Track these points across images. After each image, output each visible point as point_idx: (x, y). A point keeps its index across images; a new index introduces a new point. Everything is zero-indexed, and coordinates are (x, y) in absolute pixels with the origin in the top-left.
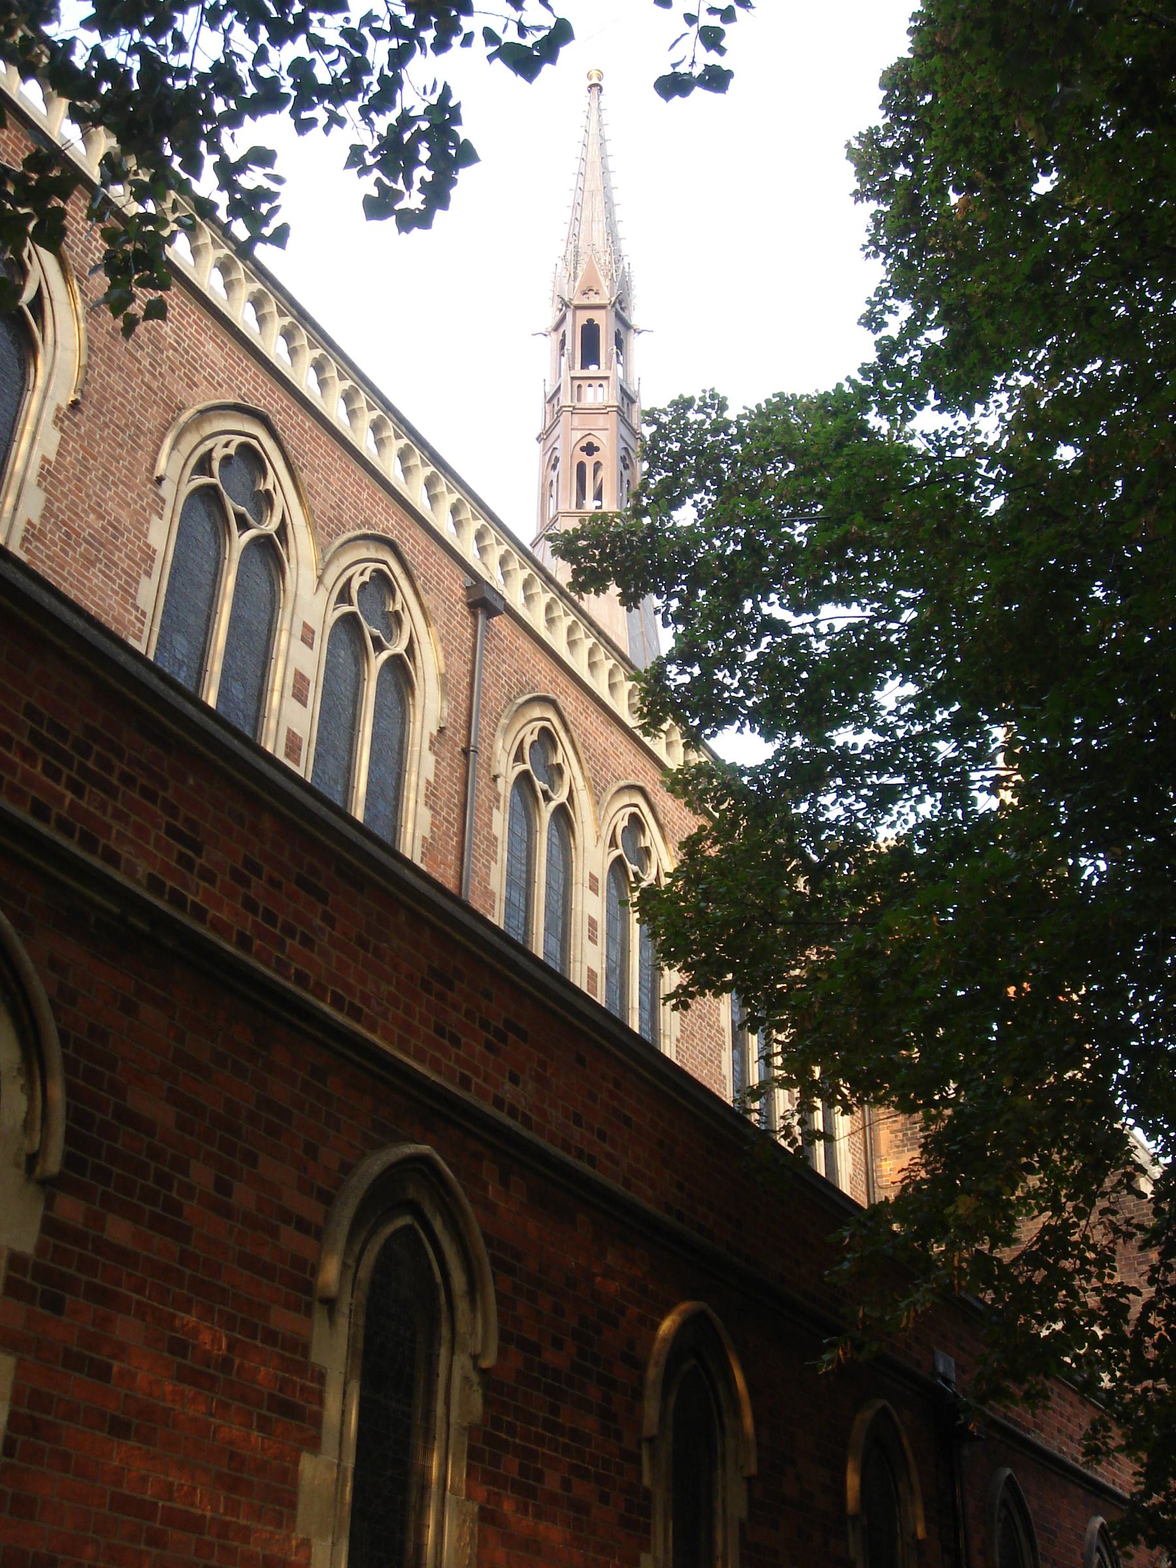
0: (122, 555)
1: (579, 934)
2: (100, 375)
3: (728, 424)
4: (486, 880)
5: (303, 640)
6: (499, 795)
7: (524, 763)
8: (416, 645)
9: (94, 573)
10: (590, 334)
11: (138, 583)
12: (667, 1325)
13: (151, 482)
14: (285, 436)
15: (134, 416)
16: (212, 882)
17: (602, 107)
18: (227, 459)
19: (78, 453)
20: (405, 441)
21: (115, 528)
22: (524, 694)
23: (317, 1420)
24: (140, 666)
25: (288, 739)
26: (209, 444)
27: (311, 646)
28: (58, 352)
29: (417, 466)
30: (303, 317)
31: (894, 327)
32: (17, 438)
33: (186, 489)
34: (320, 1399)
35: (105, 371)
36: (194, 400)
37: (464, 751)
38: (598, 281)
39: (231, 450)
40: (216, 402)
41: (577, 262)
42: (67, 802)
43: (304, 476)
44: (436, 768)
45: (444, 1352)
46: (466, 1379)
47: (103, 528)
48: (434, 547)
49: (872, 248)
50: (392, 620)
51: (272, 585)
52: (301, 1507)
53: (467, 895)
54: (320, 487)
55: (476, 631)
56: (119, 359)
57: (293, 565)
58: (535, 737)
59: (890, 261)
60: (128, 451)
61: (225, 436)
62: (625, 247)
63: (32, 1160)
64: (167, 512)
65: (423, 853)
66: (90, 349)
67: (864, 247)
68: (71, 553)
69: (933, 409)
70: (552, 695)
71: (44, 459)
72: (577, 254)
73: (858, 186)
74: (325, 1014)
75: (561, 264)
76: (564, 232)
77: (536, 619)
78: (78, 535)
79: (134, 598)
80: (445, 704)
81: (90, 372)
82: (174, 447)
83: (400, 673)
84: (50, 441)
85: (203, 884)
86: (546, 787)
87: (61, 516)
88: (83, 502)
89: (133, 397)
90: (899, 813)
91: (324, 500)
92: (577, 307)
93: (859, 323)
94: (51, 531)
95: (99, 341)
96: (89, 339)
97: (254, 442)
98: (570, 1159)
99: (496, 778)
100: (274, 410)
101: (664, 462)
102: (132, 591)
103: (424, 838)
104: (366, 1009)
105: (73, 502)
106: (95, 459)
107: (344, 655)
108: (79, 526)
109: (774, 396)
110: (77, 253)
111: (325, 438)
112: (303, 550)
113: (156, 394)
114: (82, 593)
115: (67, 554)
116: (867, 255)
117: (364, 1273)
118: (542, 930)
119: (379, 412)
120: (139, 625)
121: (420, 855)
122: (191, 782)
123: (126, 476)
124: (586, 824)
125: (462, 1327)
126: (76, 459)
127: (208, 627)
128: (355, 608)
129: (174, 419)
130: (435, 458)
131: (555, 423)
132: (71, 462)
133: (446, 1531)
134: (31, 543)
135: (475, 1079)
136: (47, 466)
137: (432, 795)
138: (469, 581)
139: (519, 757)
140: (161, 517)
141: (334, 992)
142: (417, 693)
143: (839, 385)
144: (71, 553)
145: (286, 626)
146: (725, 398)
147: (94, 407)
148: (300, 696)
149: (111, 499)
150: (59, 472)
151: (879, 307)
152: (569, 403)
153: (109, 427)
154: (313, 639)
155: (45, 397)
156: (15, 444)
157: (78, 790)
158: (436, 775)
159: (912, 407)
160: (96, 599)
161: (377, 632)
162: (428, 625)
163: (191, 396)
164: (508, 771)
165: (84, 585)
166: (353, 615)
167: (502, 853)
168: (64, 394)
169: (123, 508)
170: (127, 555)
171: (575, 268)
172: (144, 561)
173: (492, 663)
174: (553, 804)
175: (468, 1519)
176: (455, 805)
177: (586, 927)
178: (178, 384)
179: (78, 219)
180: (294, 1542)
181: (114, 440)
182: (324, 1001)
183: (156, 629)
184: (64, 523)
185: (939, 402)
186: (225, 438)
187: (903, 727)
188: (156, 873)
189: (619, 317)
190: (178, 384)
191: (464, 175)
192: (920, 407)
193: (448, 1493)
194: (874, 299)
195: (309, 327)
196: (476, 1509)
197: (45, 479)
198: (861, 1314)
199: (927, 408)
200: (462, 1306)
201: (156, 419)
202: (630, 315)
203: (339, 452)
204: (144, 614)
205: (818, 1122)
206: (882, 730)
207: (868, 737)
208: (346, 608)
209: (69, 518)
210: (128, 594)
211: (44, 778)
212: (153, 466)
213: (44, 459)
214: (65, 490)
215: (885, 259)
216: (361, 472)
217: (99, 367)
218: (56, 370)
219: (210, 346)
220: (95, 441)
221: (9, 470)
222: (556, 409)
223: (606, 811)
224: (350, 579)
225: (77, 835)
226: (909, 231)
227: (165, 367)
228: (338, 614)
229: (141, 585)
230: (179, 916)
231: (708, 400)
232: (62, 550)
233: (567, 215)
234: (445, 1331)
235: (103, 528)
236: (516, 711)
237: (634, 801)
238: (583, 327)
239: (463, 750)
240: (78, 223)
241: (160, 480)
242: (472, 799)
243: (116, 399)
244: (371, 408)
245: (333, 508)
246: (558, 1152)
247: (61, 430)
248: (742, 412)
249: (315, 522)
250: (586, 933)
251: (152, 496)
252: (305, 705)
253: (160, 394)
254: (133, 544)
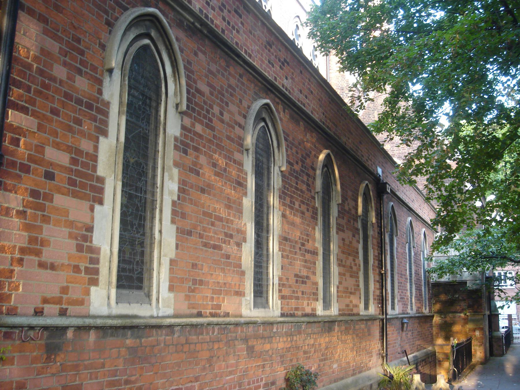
125: (276, 158)
200: (276, 151)
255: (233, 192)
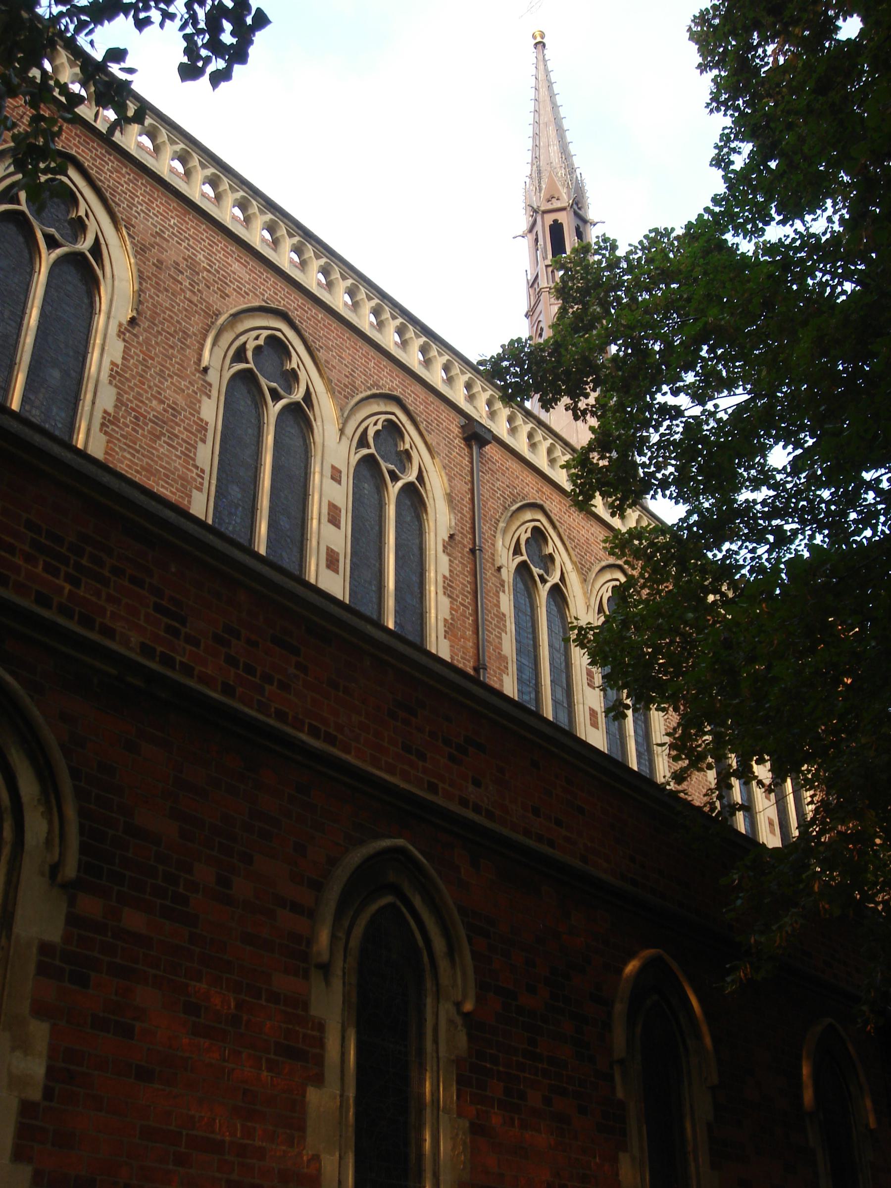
0: (182, 429)
1: (580, 683)
2: (150, 296)
3: (619, 259)
4: (499, 647)
5: (332, 478)
6: (504, 581)
7: (522, 555)
8: (425, 474)
9: (160, 445)
10: (556, 230)
11: (196, 448)
12: (631, 967)
13: (199, 372)
14: (303, 326)
15: (181, 324)
16: (197, 644)
17: (547, 58)
18: (258, 349)
19: (139, 356)
20: (400, 320)
21: (173, 409)
22: (516, 503)
23: (320, 1061)
24: (124, 484)
25: (327, 554)
26: (242, 339)
27: (339, 482)
28: (116, 283)
29: (412, 338)
30: (307, 235)
31: (739, 162)
32: (90, 350)
33: (227, 375)
34: (321, 1043)
35: (154, 293)
36: (228, 307)
37: (471, 549)
38: (558, 190)
39: (261, 342)
40: (244, 306)
41: (540, 179)
42: (66, 591)
43: (321, 355)
44: (450, 566)
45: (429, 1001)
46: (451, 1022)
47: (164, 410)
48: (432, 398)
49: (714, 104)
50: (404, 456)
51: (305, 440)
52: (309, 1130)
53: (484, 660)
54: (334, 362)
55: (472, 458)
56: (165, 283)
57: (319, 423)
58: (529, 534)
59: (730, 112)
60: (178, 351)
61: (254, 332)
62: (577, 162)
63: (55, 869)
64: (214, 393)
65: (445, 631)
66: (140, 277)
67: (708, 105)
68: (140, 431)
69: (778, 223)
70: (539, 501)
71: (113, 363)
72: (539, 172)
73: (700, 60)
74: (303, 742)
75: (528, 180)
76: (528, 157)
77: (521, 444)
78: (145, 417)
79: (194, 460)
80: (452, 517)
81: (142, 295)
82: (214, 343)
83: (414, 497)
84: (116, 350)
85: (188, 647)
86: (541, 572)
87: (130, 405)
88: (147, 392)
89: (178, 310)
90: (795, 550)
91: (339, 371)
92: (544, 212)
93: (711, 165)
94: (123, 416)
95: (148, 271)
96: (139, 271)
97: (279, 334)
98: (531, 843)
99: (499, 569)
100: (292, 308)
101: (574, 298)
102: (192, 455)
103: (445, 620)
104: (340, 736)
105: (138, 393)
106: (153, 359)
107: (368, 487)
108: (145, 411)
109: (650, 231)
110: (123, 208)
111: (335, 324)
112: (326, 411)
113: (196, 306)
114: (152, 460)
115: (137, 432)
116: (711, 111)
117: (355, 942)
118: (548, 682)
119: (376, 301)
120: (199, 480)
121: (443, 633)
122: (173, 570)
123: (178, 370)
124: (577, 598)
125: (445, 981)
126: (137, 360)
127: (256, 477)
128: (372, 450)
129: (213, 323)
130: (426, 331)
131: (537, 302)
132: (134, 364)
133: (441, 1144)
134: (108, 427)
135: (441, 785)
136: (115, 368)
137: (448, 587)
138: (463, 421)
139: (517, 551)
140: (209, 397)
141: (310, 725)
142: (429, 510)
143: (700, 216)
144: (140, 431)
145: (318, 469)
146: (615, 241)
147: (148, 320)
148: (334, 520)
149: (168, 387)
150: (126, 372)
151: (726, 150)
152: (546, 285)
153: (162, 335)
154: (340, 477)
155: (109, 318)
156: (89, 355)
157: (75, 582)
158: (450, 571)
159: (760, 225)
160: (164, 464)
161: (392, 467)
162: (433, 457)
163: (225, 304)
164: (509, 563)
165: (153, 454)
166: (371, 456)
167: (511, 626)
168: (124, 312)
169: (178, 394)
170: (185, 428)
171: (540, 183)
172: (199, 432)
173: (488, 481)
174: (548, 585)
175: (461, 1133)
176: (468, 592)
177: (585, 676)
178: (213, 296)
179: (122, 183)
180: (305, 1158)
181: (167, 344)
182: (302, 731)
183: (214, 482)
184: (133, 409)
185: (781, 217)
186: (254, 334)
187: (791, 482)
188: (147, 642)
189: (576, 214)
190: (213, 296)
191: (259, 37)
192: (767, 223)
193: (441, 1113)
194: (720, 144)
195: (313, 243)
196: (467, 1124)
197: (114, 378)
198: (752, 940)
199: (773, 223)
200: (443, 965)
201: (198, 324)
202: (586, 213)
203: (348, 334)
204: (203, 471)
205: (737, 795)
206: (775, 486)
207: (765, 493)
208: (365, 451)
209: (137, 405)
210: (189, 457)
211: (45, 575)
212: (200, 360)
213: (113, 363)
214: (132, 385)
215: (725, 111)
216: (366, 348)
217: (149, 290)
218: (115, 297)
219: (236, 266)
220: (152, 346)
221: (86, 375)
222: (537, 290)
223: (593, 585)
224: (366, 429)
225: (76, 617)
226: (737, 82)
227: (202, 286)
228: (359, 456)
229: (198, 450)
230: (169, 673)
231: (602, 244)
232: (133, 429)
233: (529, 144)
234: (429, 984)
235: (164, 410)
236: (512, 516)
237: (615, 577)
238: (551, 226)
239: (471, 550)
240: (123, 186)
241: (206, 370)
242: (481, 586)
243: (165, 313)
244: (370, 299)
245: (347, 377)
246: (520, 838)
247: (124, 340)
248: (630, 248)
249: (334, 388)
250: (585, 681)
251: (201, 382)
252: (339, 527)
253: (199, 305)
254: (190, 419)
255: (265, 1073)
